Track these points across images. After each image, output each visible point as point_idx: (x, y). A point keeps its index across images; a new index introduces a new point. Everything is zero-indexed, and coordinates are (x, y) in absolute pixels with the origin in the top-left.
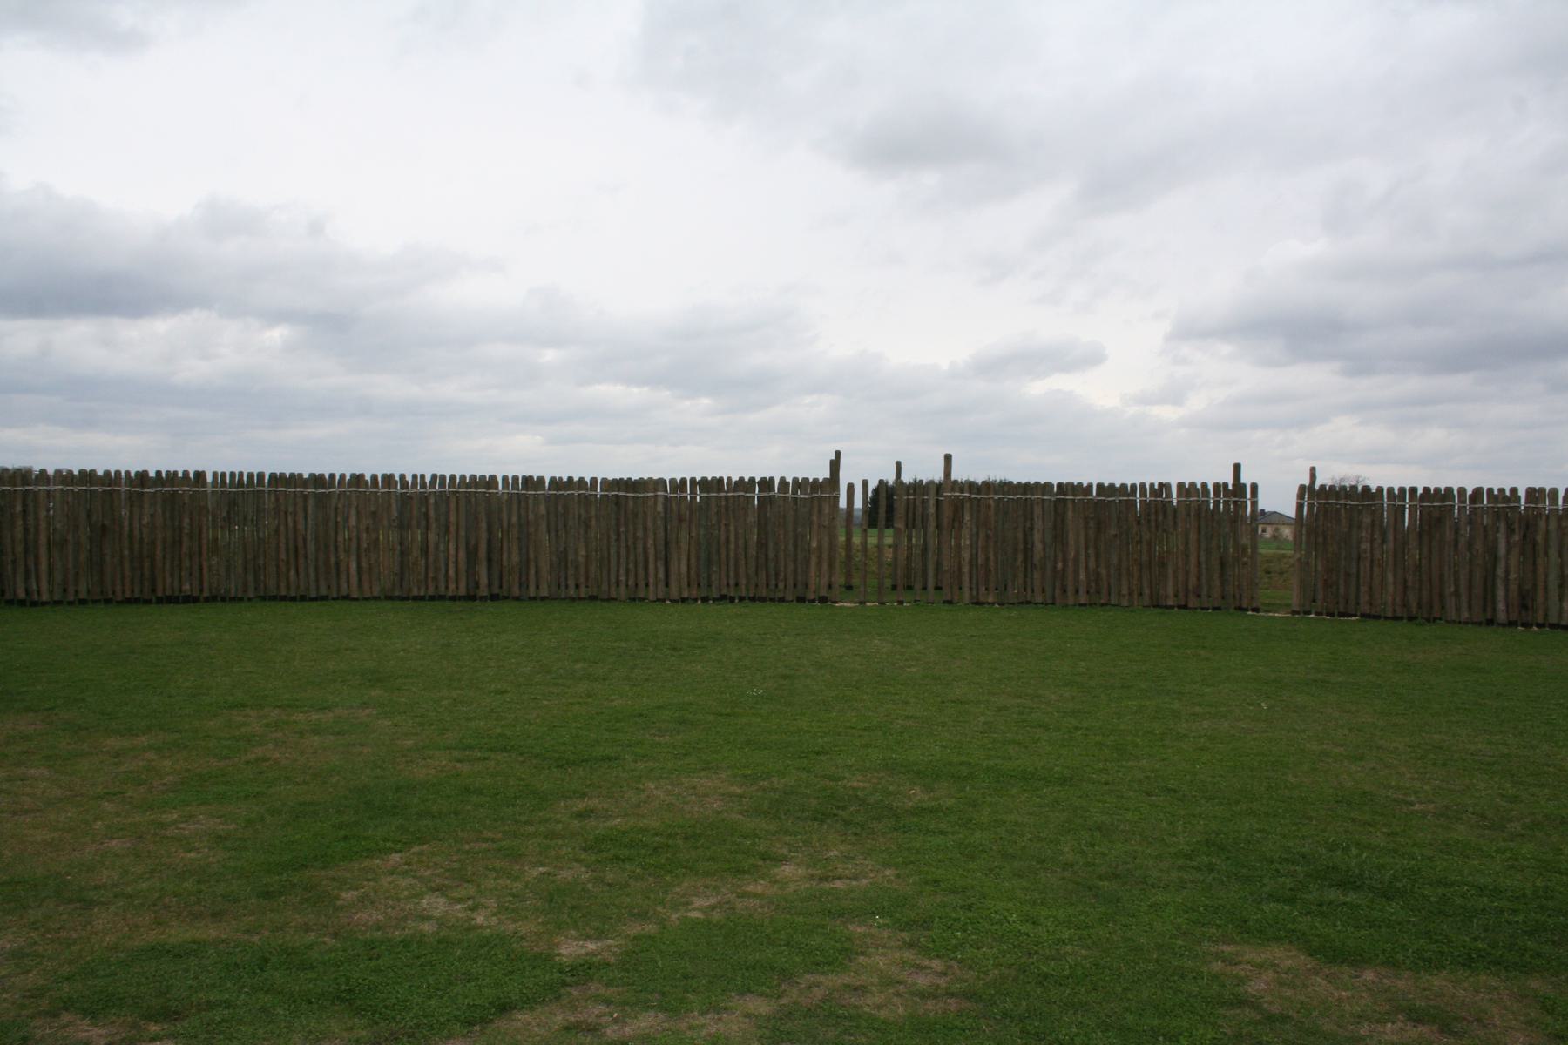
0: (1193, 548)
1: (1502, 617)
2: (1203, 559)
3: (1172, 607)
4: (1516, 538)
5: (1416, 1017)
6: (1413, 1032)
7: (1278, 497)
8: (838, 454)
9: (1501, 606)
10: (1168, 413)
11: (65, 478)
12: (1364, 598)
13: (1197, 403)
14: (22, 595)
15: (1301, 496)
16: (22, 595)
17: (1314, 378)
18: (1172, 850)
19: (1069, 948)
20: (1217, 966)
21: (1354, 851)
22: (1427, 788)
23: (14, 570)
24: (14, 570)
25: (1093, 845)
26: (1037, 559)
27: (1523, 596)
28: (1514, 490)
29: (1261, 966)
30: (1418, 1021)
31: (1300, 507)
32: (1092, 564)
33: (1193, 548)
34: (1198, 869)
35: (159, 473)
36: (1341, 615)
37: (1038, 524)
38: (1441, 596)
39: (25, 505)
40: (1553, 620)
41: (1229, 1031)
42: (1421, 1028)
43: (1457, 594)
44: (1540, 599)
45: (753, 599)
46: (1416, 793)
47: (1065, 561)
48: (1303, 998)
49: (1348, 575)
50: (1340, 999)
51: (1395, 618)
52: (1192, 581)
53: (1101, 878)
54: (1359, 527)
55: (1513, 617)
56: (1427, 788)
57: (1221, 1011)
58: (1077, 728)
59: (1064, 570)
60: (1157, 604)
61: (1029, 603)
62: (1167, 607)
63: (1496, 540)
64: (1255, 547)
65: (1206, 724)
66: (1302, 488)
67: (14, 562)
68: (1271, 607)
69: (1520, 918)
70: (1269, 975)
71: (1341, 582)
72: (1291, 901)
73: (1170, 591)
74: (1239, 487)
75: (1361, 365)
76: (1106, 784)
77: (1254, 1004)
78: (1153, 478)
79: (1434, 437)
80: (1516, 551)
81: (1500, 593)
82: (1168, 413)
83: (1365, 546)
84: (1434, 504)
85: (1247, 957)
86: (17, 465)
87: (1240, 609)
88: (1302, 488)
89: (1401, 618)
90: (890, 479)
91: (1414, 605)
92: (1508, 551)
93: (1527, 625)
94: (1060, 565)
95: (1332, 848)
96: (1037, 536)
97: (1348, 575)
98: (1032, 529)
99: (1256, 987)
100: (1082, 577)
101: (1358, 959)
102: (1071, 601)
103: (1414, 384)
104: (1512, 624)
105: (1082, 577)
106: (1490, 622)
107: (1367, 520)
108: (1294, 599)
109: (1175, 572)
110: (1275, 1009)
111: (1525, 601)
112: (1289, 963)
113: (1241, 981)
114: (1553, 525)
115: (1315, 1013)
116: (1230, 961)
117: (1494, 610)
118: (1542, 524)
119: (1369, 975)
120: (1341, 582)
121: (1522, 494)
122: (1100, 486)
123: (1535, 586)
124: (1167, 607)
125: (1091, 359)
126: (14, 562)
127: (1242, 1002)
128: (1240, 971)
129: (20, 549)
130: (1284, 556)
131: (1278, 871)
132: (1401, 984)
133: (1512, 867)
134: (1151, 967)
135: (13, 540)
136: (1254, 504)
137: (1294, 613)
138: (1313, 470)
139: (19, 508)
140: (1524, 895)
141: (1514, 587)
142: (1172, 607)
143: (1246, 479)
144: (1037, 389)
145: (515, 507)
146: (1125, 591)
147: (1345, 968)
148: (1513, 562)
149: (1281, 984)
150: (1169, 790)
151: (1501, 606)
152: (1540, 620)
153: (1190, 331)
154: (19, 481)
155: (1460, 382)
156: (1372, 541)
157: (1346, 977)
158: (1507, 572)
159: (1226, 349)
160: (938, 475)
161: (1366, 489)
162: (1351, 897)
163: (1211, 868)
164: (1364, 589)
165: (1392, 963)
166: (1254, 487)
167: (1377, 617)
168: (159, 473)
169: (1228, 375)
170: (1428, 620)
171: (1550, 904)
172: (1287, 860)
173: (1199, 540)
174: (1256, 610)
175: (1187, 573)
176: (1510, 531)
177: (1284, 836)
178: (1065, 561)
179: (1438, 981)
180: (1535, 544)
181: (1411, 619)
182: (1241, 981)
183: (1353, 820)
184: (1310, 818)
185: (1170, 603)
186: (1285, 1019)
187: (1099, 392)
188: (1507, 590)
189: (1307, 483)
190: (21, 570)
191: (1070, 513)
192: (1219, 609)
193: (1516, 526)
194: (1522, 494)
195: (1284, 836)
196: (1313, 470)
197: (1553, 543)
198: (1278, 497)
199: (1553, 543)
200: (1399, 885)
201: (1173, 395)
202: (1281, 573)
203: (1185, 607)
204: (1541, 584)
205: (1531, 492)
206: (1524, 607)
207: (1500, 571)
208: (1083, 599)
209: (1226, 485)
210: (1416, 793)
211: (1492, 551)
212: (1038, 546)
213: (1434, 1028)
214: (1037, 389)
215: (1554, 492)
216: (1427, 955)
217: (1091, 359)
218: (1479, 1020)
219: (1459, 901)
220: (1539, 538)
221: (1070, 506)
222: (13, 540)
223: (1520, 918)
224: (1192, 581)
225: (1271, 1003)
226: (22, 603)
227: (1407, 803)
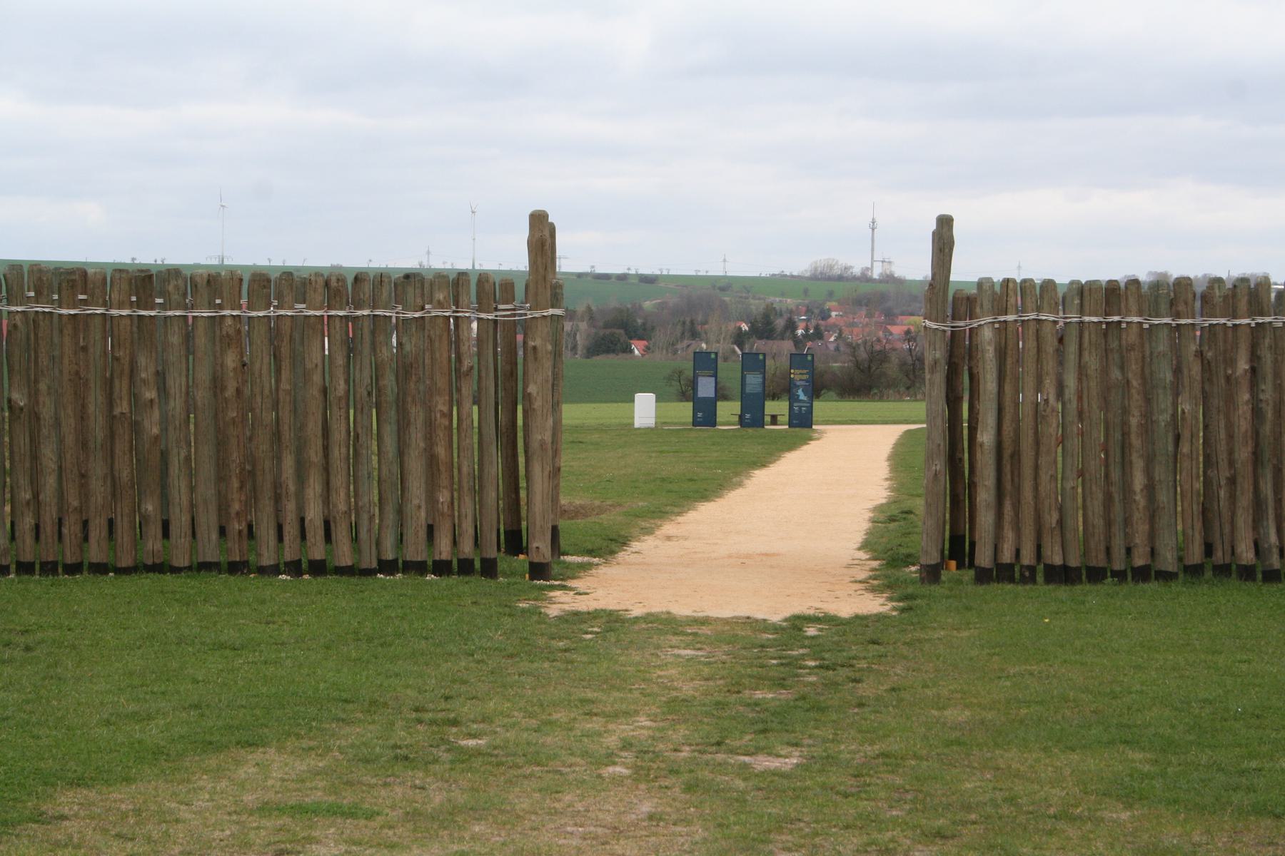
8: (945, 223)
14: (1246, 554)
16: (1246, 554)
23: (1233, 498)
24: (1233, 498)
39: (1254, 357)
45: (49, 568)
67: (1232, 481)
86: (1237, 272)
126: (1232, 481)
129: (1243, 454)
135: (1230, 437)
139: (1243, 365)
142: (275, 570)
145: (1072, 348)
154: (1243, 305)
160: (512, 256)
190: (1245, 500)
222: (1230, 437)
226: (1247, 573)
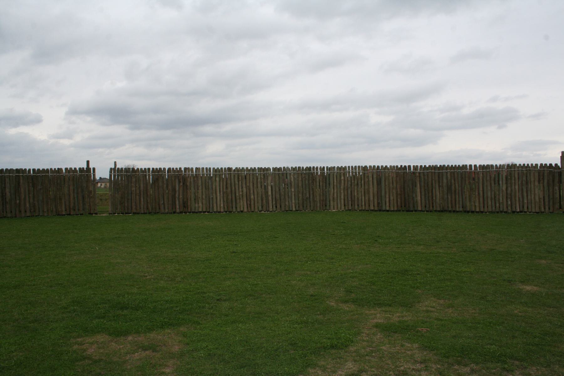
0: (71, 192)
1: (178, 211)
2: (76, 196)
3: (64, 215)
4: (181, 184)
5: (145, 349)
6: (144, 354)
7: (102, 172)
9: (178, 207)
10: (66, 142)
11: (294, 169)
12: (134, 207)
13: (78, 138)
15: (111, 172)
17: (119, 130)
18: (60, 307)
19: (15, 354)
20: (75, 347)
21: (126, 296)
22: (152, 270)
25: (27, 310)
26: (7, 200)
27: (184, 203)
28: (180, 168)
29: (92, 343)
30: (146, 350)
31: (110, 176)
32: (31, 201)
33: (71, 192)
34: (70, 312)
35: (401, 166)
36: (126, 213)
37: (8, 185)
38: (159, 205)
40: (193, 210)
41: (79, 370)
42: (147, 352)
43: (164, 204)
44: (189, 204)
46: (148, 272)
47: (20, 200)
48: (107, 351)
49: (128, 199)
50: (120, 349)
51: (145, 213)
52: (72, 205)
53: (30, 323)
54: (131, 183)
55: (181, 210)
56: (152, 270)
57: (77, 363)
58: (23, 265)
59: (20, 203)
60: (59, 214)
61: (5, 217)
62: (63, 215)
63: (175, 185)
64: (95, 191)
65: (75, 257)
66: (111, 169)
68: (103, 212)
69: (178, 309)
70: (96, 345)
71: (126, 202)
72: (104, 318)
73: (64, 209)
74: (88, 168)
75: (136, 126)
76: (34, 285)
77: (89, 358)
78: (55, 166)
79: (160, 151)
80: (181, 188)
81: (177, 203)
82: (66, 142)
83: (134, 189)
84: (158, 172)
85: (87, 341)
87: (90, 214)
88: (111, 169)
89: (146, 213)
90: (85, 166)
91: (150, 208)
92: (179, 189)
93: (185, 213)
94: (18, 201)
95: (118, 296)
96: (7, 190)
97: (128, 199)
98: (5, 188)
99: (90, 352)
100: (28, 205)
101: (126, 333)
102: (283, 209)
103: (154, 133)
104: (181, 212)
105: (28, 205)
106: (175, 212)
107: (134, 180)
108: (110, 209)
109: (65, 202)
110: (97, 358)
111: (185, 205)
112: (102, 340)
113: (85, 351)
114: (192, 180)
115: (111, 356)
116: (81, 344)
117: (176, 208)
118: (189, 179)
119: (130, 338)
120: (126, 202)
121: (183, 169)
122: (34, 170)
123: (187, 199)
124: (63, 215)
125: (37, 120)
127: (84, 358)
128: (84, 347)
130: (107, 194)
131: (99, 308)
132: (140, 339)
133: (176, 293)
134: (50, 353)
136: (94, 175)
137: (110, 214)
138: (115, 162)
140: (180, 301)
141: (181, 200)
142: (64, 215)
143: (91, 166)
144: (12, 131)
146: (45, 210)
147: (122, 337)
148: (181, 191)
149: (99, 348)
150: (59, 284)
151: (178, 207)
152: (189, 211)
153: (74, 112)
155: (168, 133)
156: (136, 187)
157: (122, 340)
158: (179, 196)
159: (89, 119)
161: (133, 169)
162: (125, 312)
163: (75, 311)
164: (133, 204)
165: (138, 332)
166: (94, 169)
167: (138, 213)
168: (401, 166)
169: (89, 129)
170: (155, 213)
171: (187, 302)
172: (103, 303)
173: (74, 190)
174: (96, 214)
175: (70, 202)
176: (180, 182)
177: (102, 295)
178: (20, 200)
179: (152, 335)
180: (187, 186)
181: (149, 213)
182: (85, 351)
183: (127, 285)
184: (112, 287)
185: (64, 213)
186: (101, 360)
187: (39, 134)
188: (179, 201)
189: (113, 167)
191: (21, 181)
192: (82, 214)
193: (181, 180)
194: (183, 169)
195: (102, 295)
196: (115, 162)
197: (192, 185)
198: (102, 172)
199: (192, 185)
200: (141, 305)
201: (69, 135)
202: (106, 200)
203: (70, 214)
204: (189, 199)
205: (185, 169)
206: (184, 207)
207: (177, 195)
208: (28, 214)
209: (83, 168)
210: (148, 272)
211: (174, 190)
212: (8, 194)
213: (151, 351)
214: (12, 131)
215: (192, 169)
216: (149, 327)
217: (37, 120)
218: (165, 345)
219: (160, 307)
220: (188, 184)
221: (21, 178)
223: (178, 309)
224: (72, 205)
225: (95, 356)
227: (145, 276)
